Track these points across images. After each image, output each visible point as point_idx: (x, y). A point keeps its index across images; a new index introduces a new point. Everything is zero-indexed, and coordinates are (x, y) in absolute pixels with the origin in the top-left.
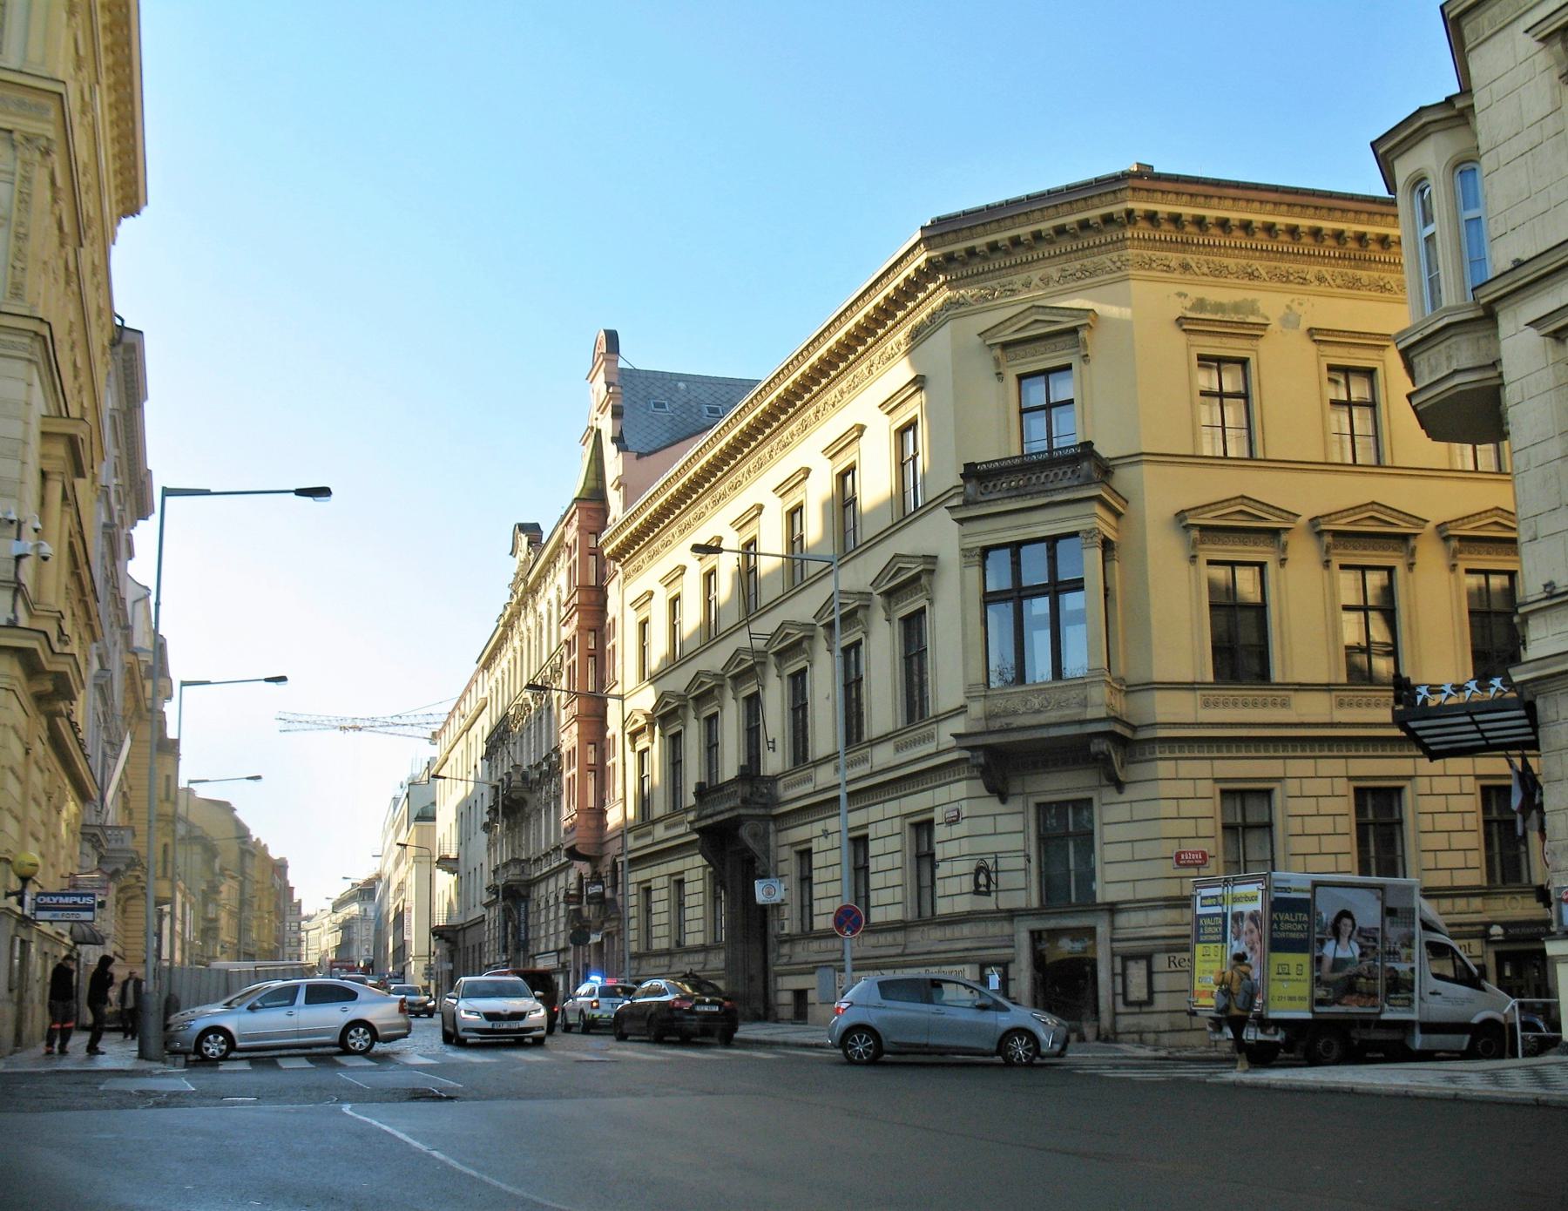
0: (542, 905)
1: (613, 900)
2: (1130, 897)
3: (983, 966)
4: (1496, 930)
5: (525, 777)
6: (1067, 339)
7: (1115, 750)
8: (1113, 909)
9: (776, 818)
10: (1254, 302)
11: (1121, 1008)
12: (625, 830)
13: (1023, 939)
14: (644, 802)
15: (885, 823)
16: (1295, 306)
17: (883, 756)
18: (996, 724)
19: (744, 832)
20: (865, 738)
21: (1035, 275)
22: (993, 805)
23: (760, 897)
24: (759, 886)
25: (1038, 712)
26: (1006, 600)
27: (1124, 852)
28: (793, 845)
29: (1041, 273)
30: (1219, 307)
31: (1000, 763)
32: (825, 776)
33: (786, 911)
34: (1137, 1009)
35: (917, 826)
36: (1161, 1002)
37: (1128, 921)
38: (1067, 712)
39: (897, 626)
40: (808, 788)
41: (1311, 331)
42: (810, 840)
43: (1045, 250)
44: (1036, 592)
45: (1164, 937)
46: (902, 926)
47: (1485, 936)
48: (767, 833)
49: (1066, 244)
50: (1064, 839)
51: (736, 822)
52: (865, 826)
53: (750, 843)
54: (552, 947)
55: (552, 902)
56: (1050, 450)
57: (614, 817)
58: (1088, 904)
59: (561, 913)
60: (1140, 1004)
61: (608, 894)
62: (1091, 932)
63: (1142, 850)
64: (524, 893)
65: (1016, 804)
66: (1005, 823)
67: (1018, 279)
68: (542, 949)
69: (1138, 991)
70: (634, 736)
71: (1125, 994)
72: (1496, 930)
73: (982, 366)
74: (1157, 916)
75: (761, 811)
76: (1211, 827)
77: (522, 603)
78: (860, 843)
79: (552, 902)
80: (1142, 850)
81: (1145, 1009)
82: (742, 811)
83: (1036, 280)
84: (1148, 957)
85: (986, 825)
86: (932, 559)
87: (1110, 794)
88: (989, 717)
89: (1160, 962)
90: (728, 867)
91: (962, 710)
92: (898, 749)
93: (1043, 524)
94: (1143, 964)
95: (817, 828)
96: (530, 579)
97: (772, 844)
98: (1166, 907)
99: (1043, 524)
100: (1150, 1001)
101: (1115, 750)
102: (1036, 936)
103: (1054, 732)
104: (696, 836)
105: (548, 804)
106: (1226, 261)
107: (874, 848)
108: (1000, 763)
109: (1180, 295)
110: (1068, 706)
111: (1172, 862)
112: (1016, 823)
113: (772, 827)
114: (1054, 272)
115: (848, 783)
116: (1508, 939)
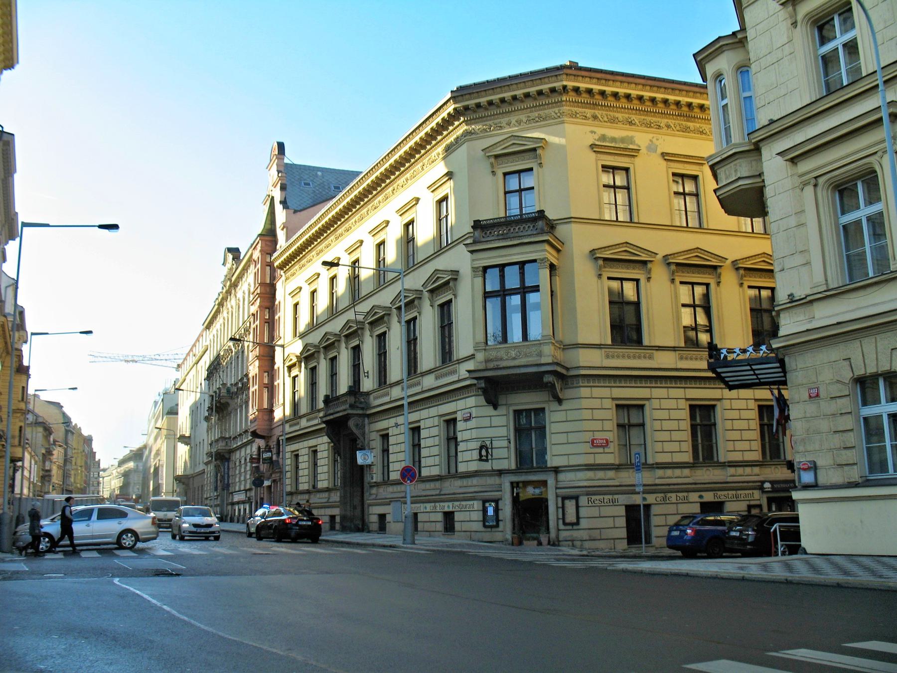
0: (238, 464)
1: (278, 461)
3: (484, 502)
4: (767, 485)
5: (228, 391)
6: (531, 154)
7: (554, 381)
8: (556, 470)
10: (632, 137)
11: (561, 527)
12: (285, 421)
13: (507, 487)
14: (295, 406)
15: (430, 420)
16: (654, 140)
17: (429, 382)
18: (491, 365)
19: (351, 423)
21: (513, 119)
22: (490, 411)
25: (514, 359)
26: (497, 296)
27: (562, 438)
29: (516, 118)
30: (613, 140)
31: (494, 387)
32: (396, 392)
34: (570, 527)
35: (448, 422)
36: (584, 523)
38: (530, 359)
40: (387, 399)
41: (663, 154)
42: (388, 429)
44: (513, 292)
45: (586, 487)
46: (439, 478)
47: (761, 488)
50: (529, 430)
51: (347, 417)
54: (242, 488)
55: (243, 462)
56: (521, 214)
57: (278, 415)
59: (248, 468)
60: (572, 524)
61: (274, 458)
62: (544, 483)
63: (572, 438)
64: (227, 456)
65: (502, 410)
66: (497, 421)
67: (504, 121)
68: (237, 489)
69: (571, 517)
70: (290, 368)
71: (564, 519)
72: (767, 485)
73: (484, 167)
74: (581, 475)
75: (360, 412)
76: (611, 425)
77: (229, 292)
78: (416, 430)
79: (243, 462)
80: (572, 438)
81: (575, 527)
82: (350, 412)
83: (513, 122)
84: (576, 498)
85: (486, 422)
86: (456, 272)
87: (554, 406)
88: (487, 361)
89: (583, 500)
91: (472, 357)
92: (437, 378)
95: (392, 421)
96: (233, 279)
100: (578, 523)
102: (514, 485)
104: (324, 425)
105: (241, 406)
107: (423, 433)
108: (494, 387)
109: (592, 132)
110: (531, 356)
111: (589, 445)
112: (502, 421)
113: (366, 420)
115: (409, 397)
116: (774, 490)
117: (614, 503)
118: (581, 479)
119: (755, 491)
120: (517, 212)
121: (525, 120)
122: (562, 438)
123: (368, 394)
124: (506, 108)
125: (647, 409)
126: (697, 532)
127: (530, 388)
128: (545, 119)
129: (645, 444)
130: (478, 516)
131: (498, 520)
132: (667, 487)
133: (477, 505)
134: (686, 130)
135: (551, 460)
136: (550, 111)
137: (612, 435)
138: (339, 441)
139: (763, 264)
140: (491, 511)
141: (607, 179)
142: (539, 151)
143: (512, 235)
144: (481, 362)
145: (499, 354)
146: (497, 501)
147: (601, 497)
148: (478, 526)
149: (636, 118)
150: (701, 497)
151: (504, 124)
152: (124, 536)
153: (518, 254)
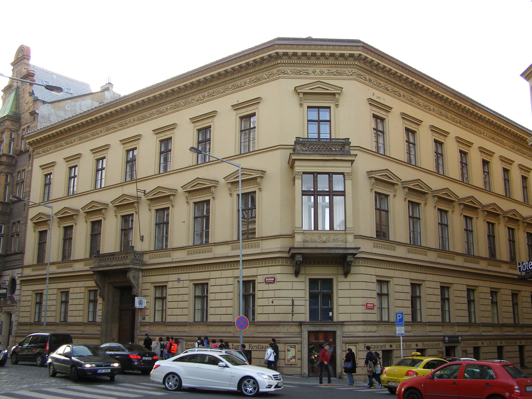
4: (447, 339)
6: (330, 97)
8: (342, 324)
9: (142, 270)
13: (305, 334)
17: (53, 269)
19: (131, 275)
22: (293, 278)
23: (137, 305)
24: (137, 300)
25: (325, 242)
27: (346, 301)
28: (152, 283)
33: (147, 312)
37: (346, 329)
43: (323, 61)
44: (323, 194)
45: (363, 337)
47: (444, 341)
48: (138, 277)
49: (331, 61)
52: (69, 288)
53: (132, 281)
56: (319, 138)
61: (8, 295)
65: (301, 278)
66: (297, 286)
67: (310, 70)
72: (447, 339)
73: (294, 100)
74: (360, 328)
76: (374, 294)
82: (131, 266)
83: (318, 71)
85: (289, 286)
87: (341, 278)
88: (305, 241)
90: (106, 289)
93: (330, 167)
95: (174, 277)
97: (140, 282)
98: (363, 325)
99: (330, 167)
101: (344, 261)
103: (333, 251)
106: (381, 82)
108: (300, 260)
111: (364, 307)
112: (301, 286)
113: (141, 274)
114: (325, 70)
116: (450, 342)
120: (316, 136)
121: (326, 72)
122: (346, 301)
123: (143, 253)
124: (313, 60)
125: (391, 284)
126: (35, 361)
127: (319, 263)
128: (340, 74)
129: (388, 308)
134: (412, 101)
135: (338, 316)
136: (345, 69)
137: (375, 301)
138: (104, 287)
141: (313, 115)
142: (337, 96)
143: (328, 153)
147: (257, 345)
149: (390, 87)
150: (417, 345)
151: (310, 72)
152: (246, 382)
153: (332, 167)
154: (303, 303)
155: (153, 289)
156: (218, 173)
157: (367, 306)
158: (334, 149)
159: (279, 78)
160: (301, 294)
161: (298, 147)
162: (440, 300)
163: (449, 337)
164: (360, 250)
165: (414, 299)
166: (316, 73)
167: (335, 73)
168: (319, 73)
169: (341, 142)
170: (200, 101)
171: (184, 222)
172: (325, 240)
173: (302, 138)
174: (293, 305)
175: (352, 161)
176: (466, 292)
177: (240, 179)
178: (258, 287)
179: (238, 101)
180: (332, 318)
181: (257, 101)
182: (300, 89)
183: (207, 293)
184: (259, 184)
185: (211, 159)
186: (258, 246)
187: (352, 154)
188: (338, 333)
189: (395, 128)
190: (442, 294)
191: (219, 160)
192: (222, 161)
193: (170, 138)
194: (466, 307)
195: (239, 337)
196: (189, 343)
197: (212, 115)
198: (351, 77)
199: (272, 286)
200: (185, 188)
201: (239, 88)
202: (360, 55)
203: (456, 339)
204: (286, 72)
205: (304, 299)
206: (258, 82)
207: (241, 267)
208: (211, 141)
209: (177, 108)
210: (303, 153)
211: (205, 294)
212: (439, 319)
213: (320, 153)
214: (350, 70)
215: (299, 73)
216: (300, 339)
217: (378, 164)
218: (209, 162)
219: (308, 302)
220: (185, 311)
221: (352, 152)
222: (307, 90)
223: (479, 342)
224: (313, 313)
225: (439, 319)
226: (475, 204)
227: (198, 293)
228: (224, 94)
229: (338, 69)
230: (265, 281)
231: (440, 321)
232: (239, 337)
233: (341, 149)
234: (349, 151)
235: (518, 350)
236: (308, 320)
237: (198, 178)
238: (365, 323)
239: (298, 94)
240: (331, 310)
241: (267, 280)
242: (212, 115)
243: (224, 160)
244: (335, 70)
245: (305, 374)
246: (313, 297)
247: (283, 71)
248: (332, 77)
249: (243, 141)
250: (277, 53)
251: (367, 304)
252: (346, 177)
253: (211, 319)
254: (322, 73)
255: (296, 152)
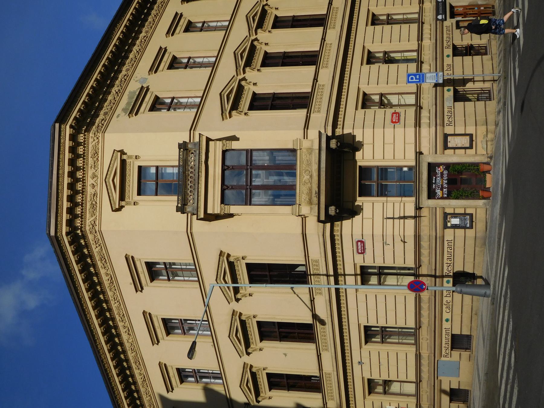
2: (413, 146)
3: (445, 227)
4: (440, 17)
10: (130, 92)
16: (136, 79)
18: (315, 200)
20: (318, 375)
21: (90, 181)
22: (357, 219)
25: (311, 176)
29: (90, 179)
30: (128, 104)
36: (471, 130)
37: (424, 150)
39: (266, 344)
44: (250, 177)
50: (381, 181)
58: (414, 170)
60: (471, 141)
62: (432, 167)
69: (464, 141)
71: (465, 148)
81: (474, 139)
84: (446, 136)
88: (310, 203)
89: (449, 130)
91: (304, 218)
94: (449, 138)
95: (357, 368)
100: (471, 136)
102: (431, 195)
103: (323, 165)
109: (118, 116)
111: (396, 125)
117: (452, 114)
118: (427, 133)
119: (444, 25)
128: (97, 153)
129: (399, 94)
130: (460, 232)
131: (465, 214)
132: (438, 60)
133: (449, 234)
136: (90, 146)
137: (389, 111)
139: (226, 278)
140: (455, 221)
143: (197, 171)
144: (311, 209)
145: (305, 192)
146: (446, 216)
148: (470, 233)
150: (448, 56)
151: (93, 191)
154: (390, 205)
155: (373, 397)
156: (222, 310)
157: (395, 122)
158: (192, 163)
159: (100, 232)
160: (378, 207)
161: (189, 209)
162: (390, 26)
163: (437, 14)
164: (323, 131)
165: (388, 59)
166: (95, 184)
167: (95, 159)
168: (95, 179)
169: (183, 154)
170: (130, 331)
171: (285, 355)
172: (308, 177)
173: (178, 203)
174: (393, 218)
175: (208, 140)
176: (376, 27)
177: (231, 285)
178: (369, 262)
179: (131, 284)
180: (410, 168)
181: (130, 261)
182: (115, 204)
183: (377, 327)
184: (237, 259)
185: (205, 319)
186: (317, 261)
187: (198, 141)
188: (431, 160)
189: (165, 83)
190: (382, 23)
191: (206, 311)
192: (207, 305)
193: (178, 370)
194: (396, 27)
195: (435, 291)
196: (443, 353)
197: (148, 317)
198: (100, 138)
199: (369, 245)
200: (242, 353)
201: (113, 279)
202: (71, 127)
203: (440, 4)
204: (93, 223)
205: (385, 204)
206: (106, 259)
207: (344, 287)
208: (182, 318)
209: (140, 362)
210: (196, 203)
211: (378, 329)
212: (414, 27)
213: (197, 181)
214: (91, 140)
215: (93, 206)
216: (438, 209)
217: (213, 104)
218: (208, 321)
219: (389, 199)
220: (402, 356)
221: (197, 140)
222: (116, 196)
223: (444, 327)
224: (403, 193)
225: (414, 27)
226: (256, 15)
227: (380, 389)
228: (122, 302)
229: (90, 155)
230: (361, 253)
231: (416, 25)
232: (435, 291)
233: (192, 153)
234: (195, 144)
235: (463, 333)
236: (413, 199)
237: (229, 337)
238: (418, 123)
239: (120, 208)
240: (400, 168)
241: (360, 251)
242: (148, 317)
243: (206, 305)
244: (90, 160)
245: (485, 204)
246: (383, 192)
247: (91, 226)
248: (99, 162)
249: (182, 278)
250: (67, 234)
251: (392, 122)
252: (227, 148)
253: (411, 323)
254: (94, 176)
255: (195, 212)
